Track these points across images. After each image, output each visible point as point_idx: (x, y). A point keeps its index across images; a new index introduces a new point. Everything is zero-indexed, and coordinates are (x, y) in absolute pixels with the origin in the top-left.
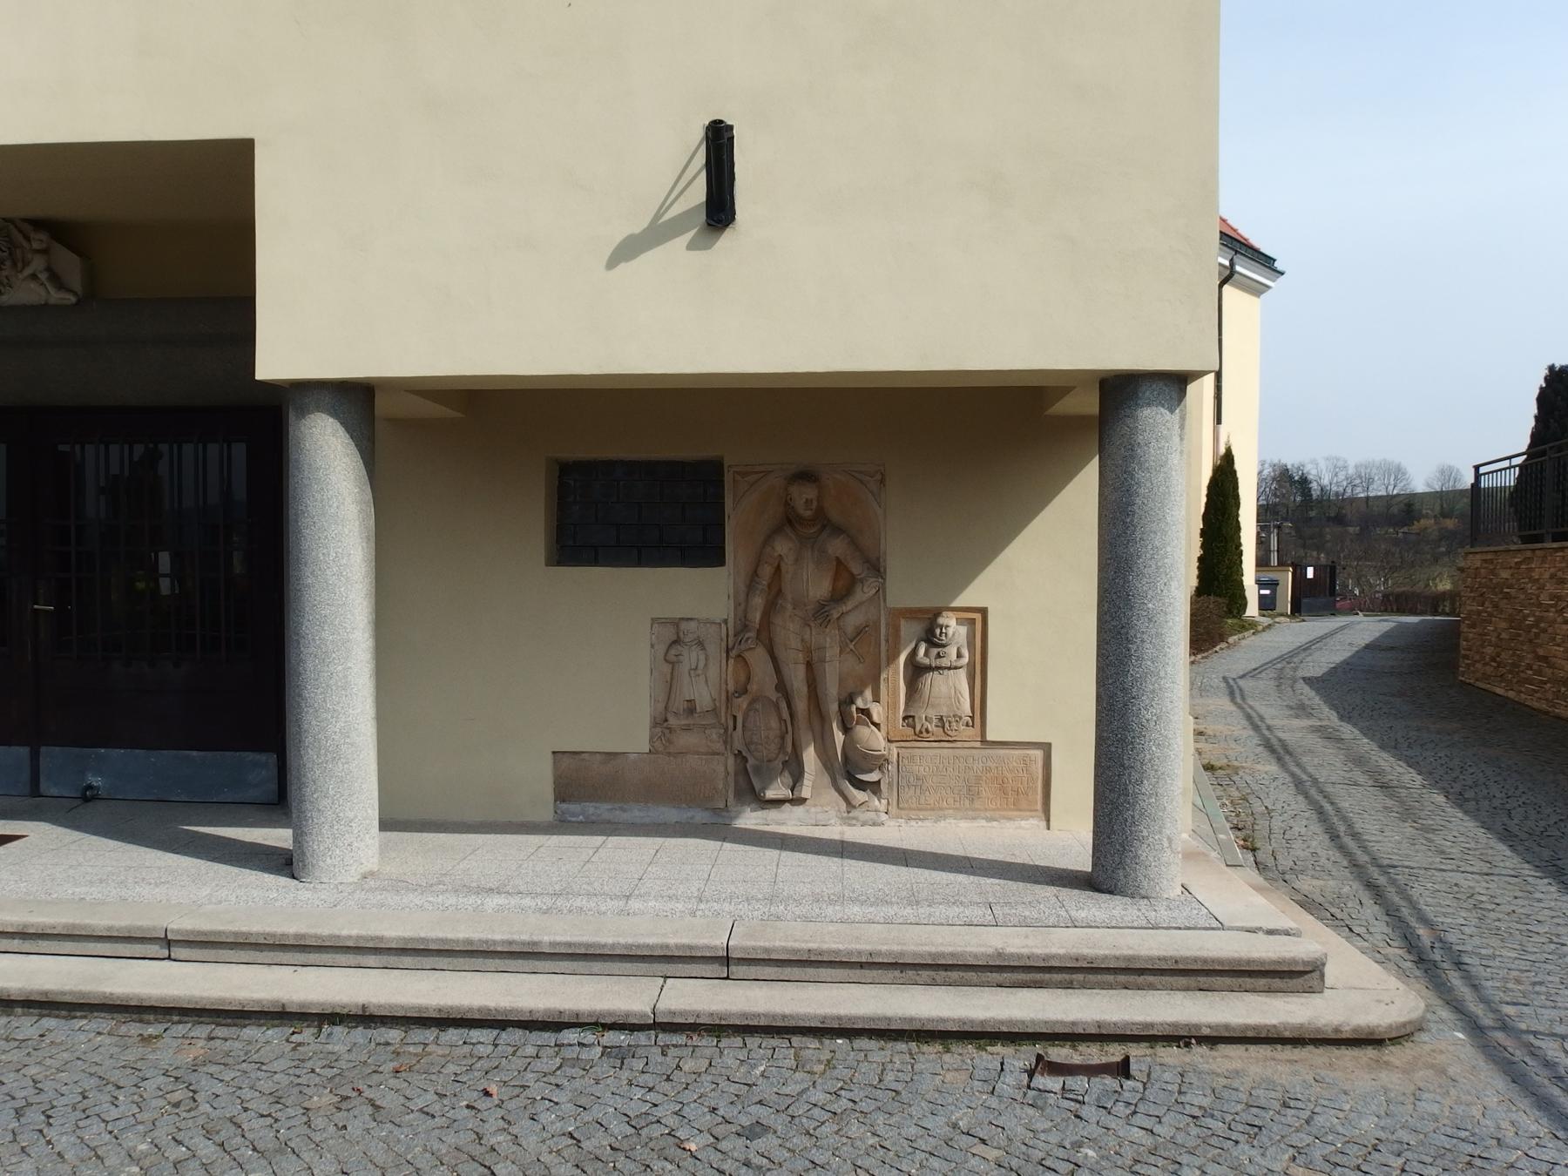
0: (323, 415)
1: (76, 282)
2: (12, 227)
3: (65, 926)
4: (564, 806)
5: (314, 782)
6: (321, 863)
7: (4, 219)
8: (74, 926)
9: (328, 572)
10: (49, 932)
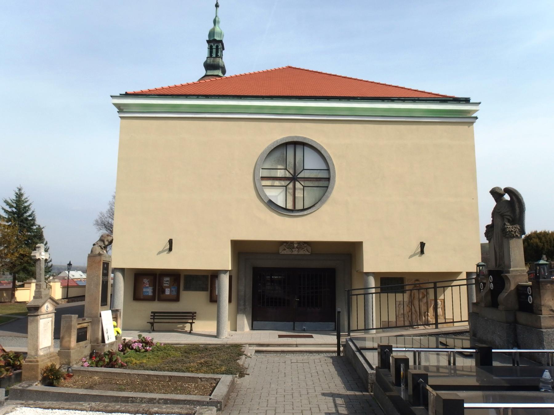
1: (310, 250)
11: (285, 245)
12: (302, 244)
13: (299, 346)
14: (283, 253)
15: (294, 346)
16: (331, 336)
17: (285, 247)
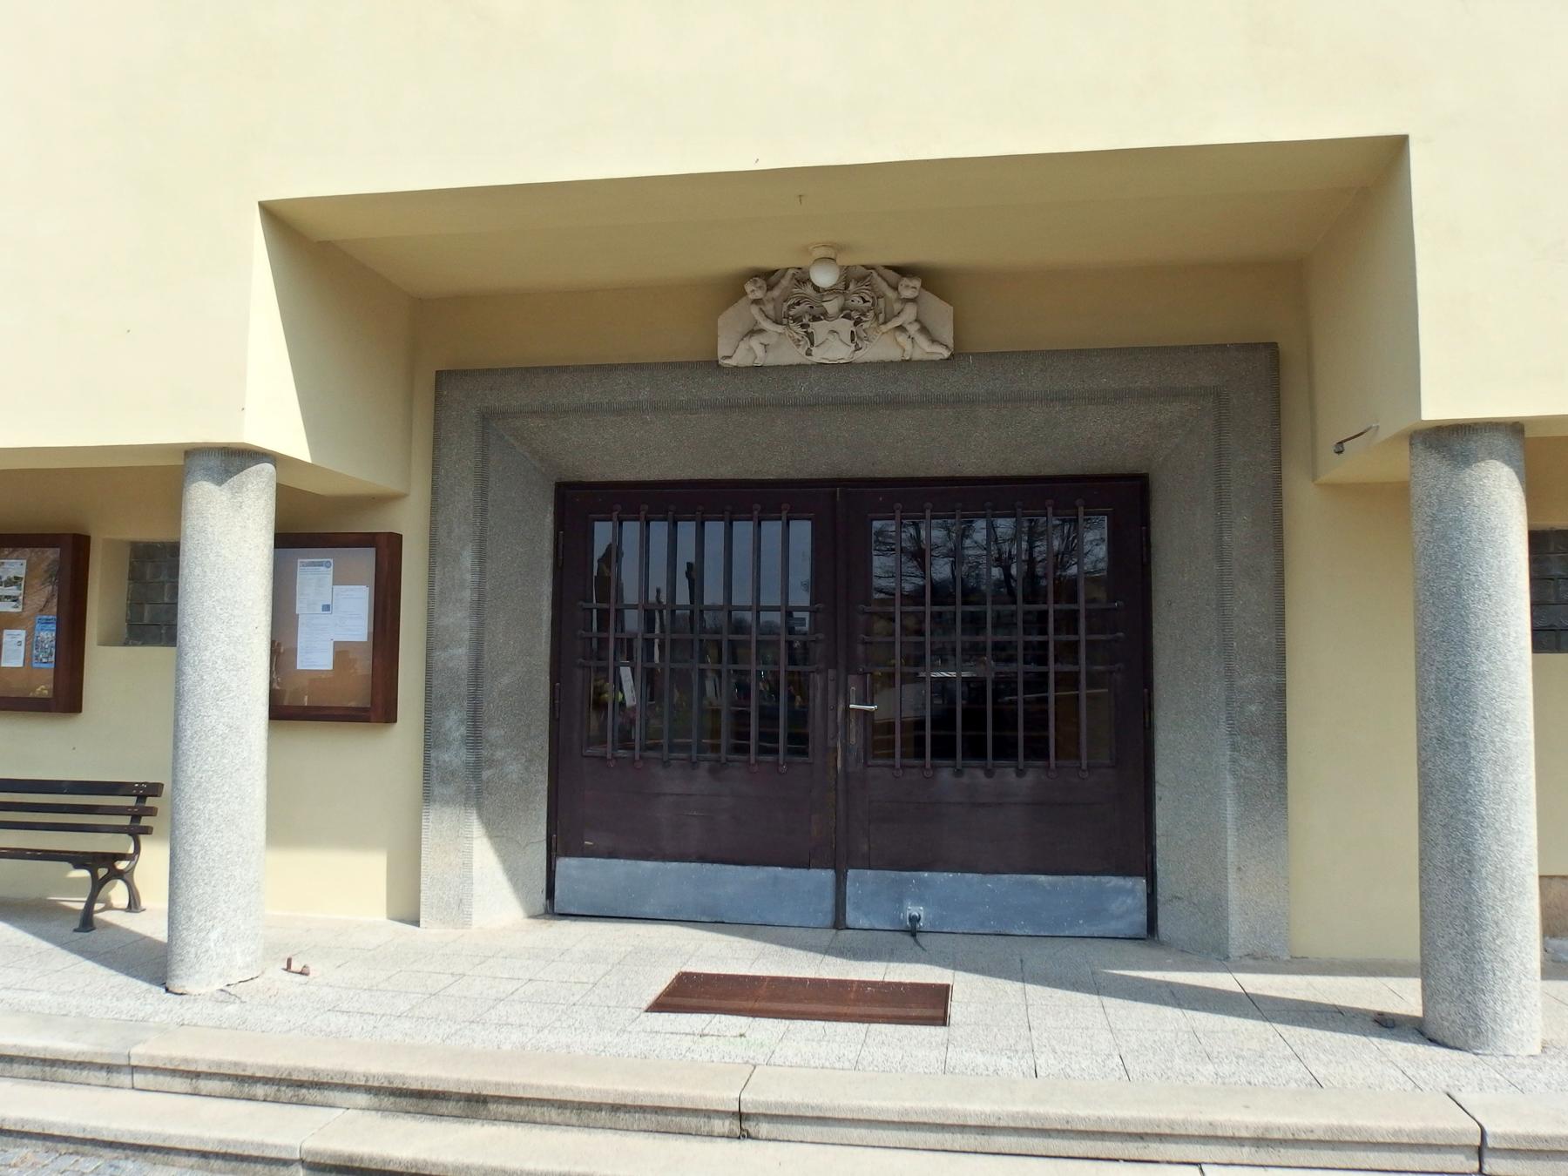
0: (1498, 463)
2: (875, 274)
3: (1329, 1129)
4: (1555, 942)
5: (1497, 923)
6: (1507, 1030)
7: (863, 266)
8: (1341, 1129)
9: (1508, 657)
10: (1304, 1136)
11: (759, 294)
12: (884, 286)
13: (764, 1128)
14: (741, 358)
15: (720, 1125)
16: (1111, 1003)
17: (755, 310)
